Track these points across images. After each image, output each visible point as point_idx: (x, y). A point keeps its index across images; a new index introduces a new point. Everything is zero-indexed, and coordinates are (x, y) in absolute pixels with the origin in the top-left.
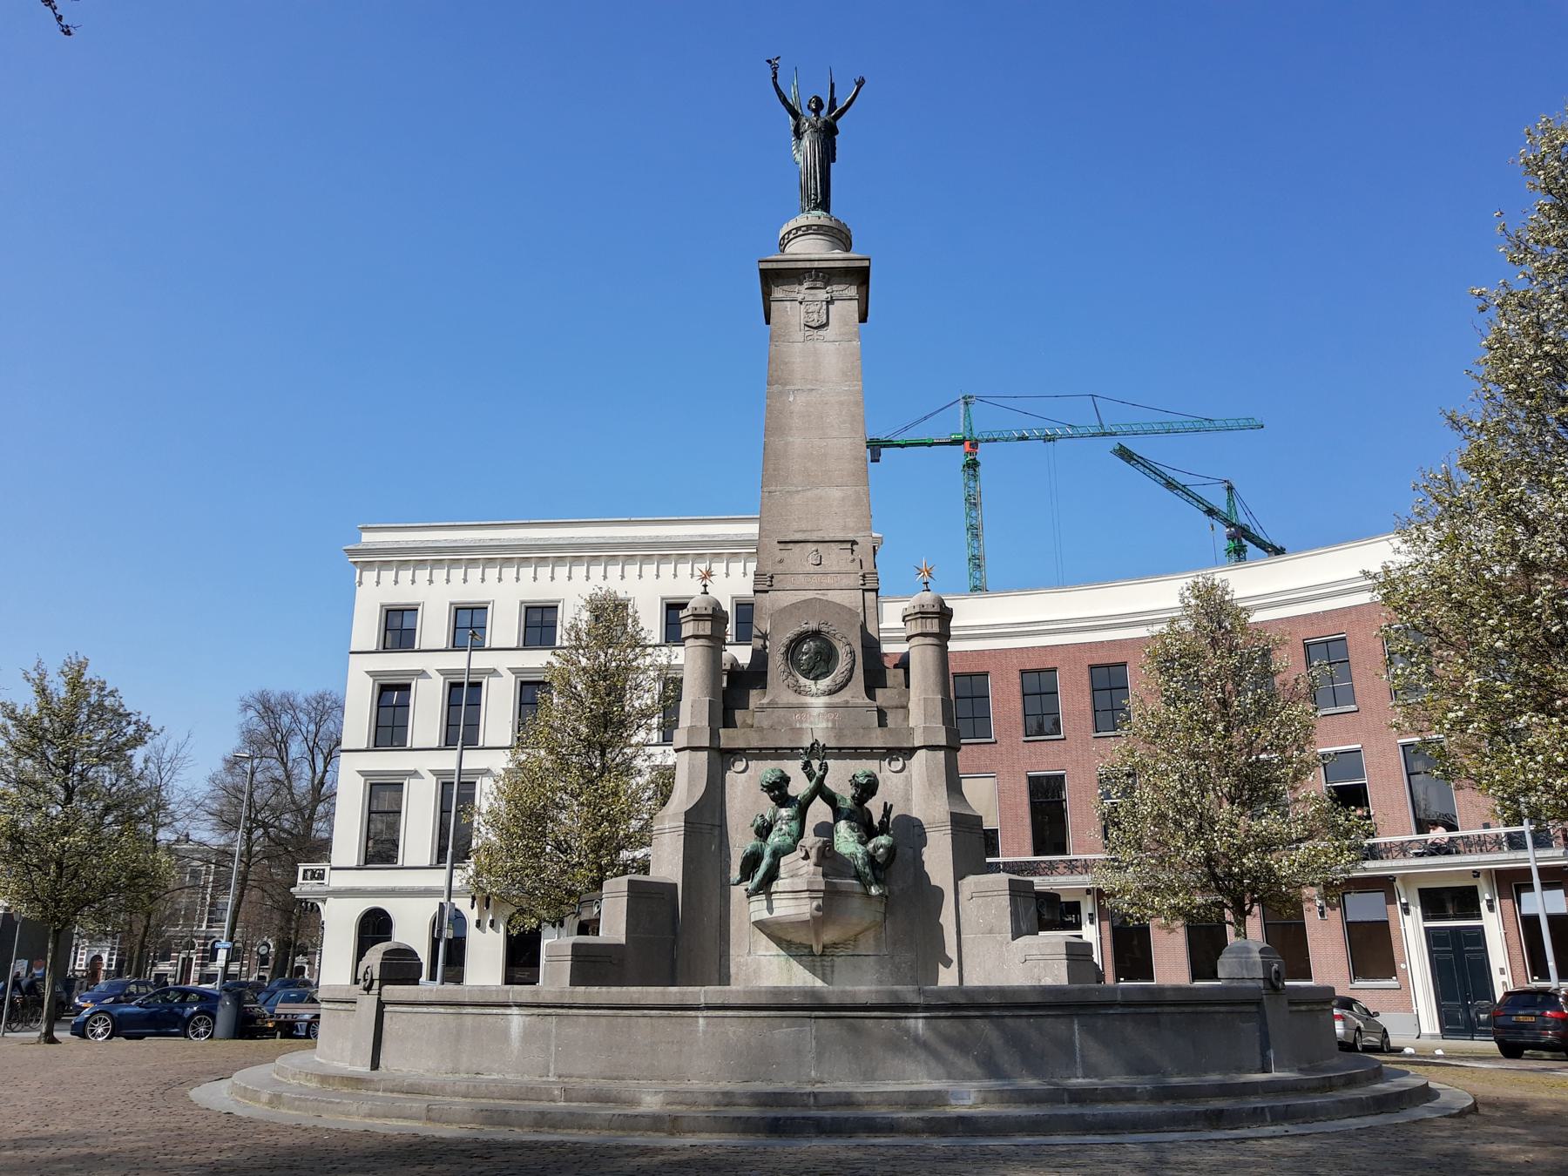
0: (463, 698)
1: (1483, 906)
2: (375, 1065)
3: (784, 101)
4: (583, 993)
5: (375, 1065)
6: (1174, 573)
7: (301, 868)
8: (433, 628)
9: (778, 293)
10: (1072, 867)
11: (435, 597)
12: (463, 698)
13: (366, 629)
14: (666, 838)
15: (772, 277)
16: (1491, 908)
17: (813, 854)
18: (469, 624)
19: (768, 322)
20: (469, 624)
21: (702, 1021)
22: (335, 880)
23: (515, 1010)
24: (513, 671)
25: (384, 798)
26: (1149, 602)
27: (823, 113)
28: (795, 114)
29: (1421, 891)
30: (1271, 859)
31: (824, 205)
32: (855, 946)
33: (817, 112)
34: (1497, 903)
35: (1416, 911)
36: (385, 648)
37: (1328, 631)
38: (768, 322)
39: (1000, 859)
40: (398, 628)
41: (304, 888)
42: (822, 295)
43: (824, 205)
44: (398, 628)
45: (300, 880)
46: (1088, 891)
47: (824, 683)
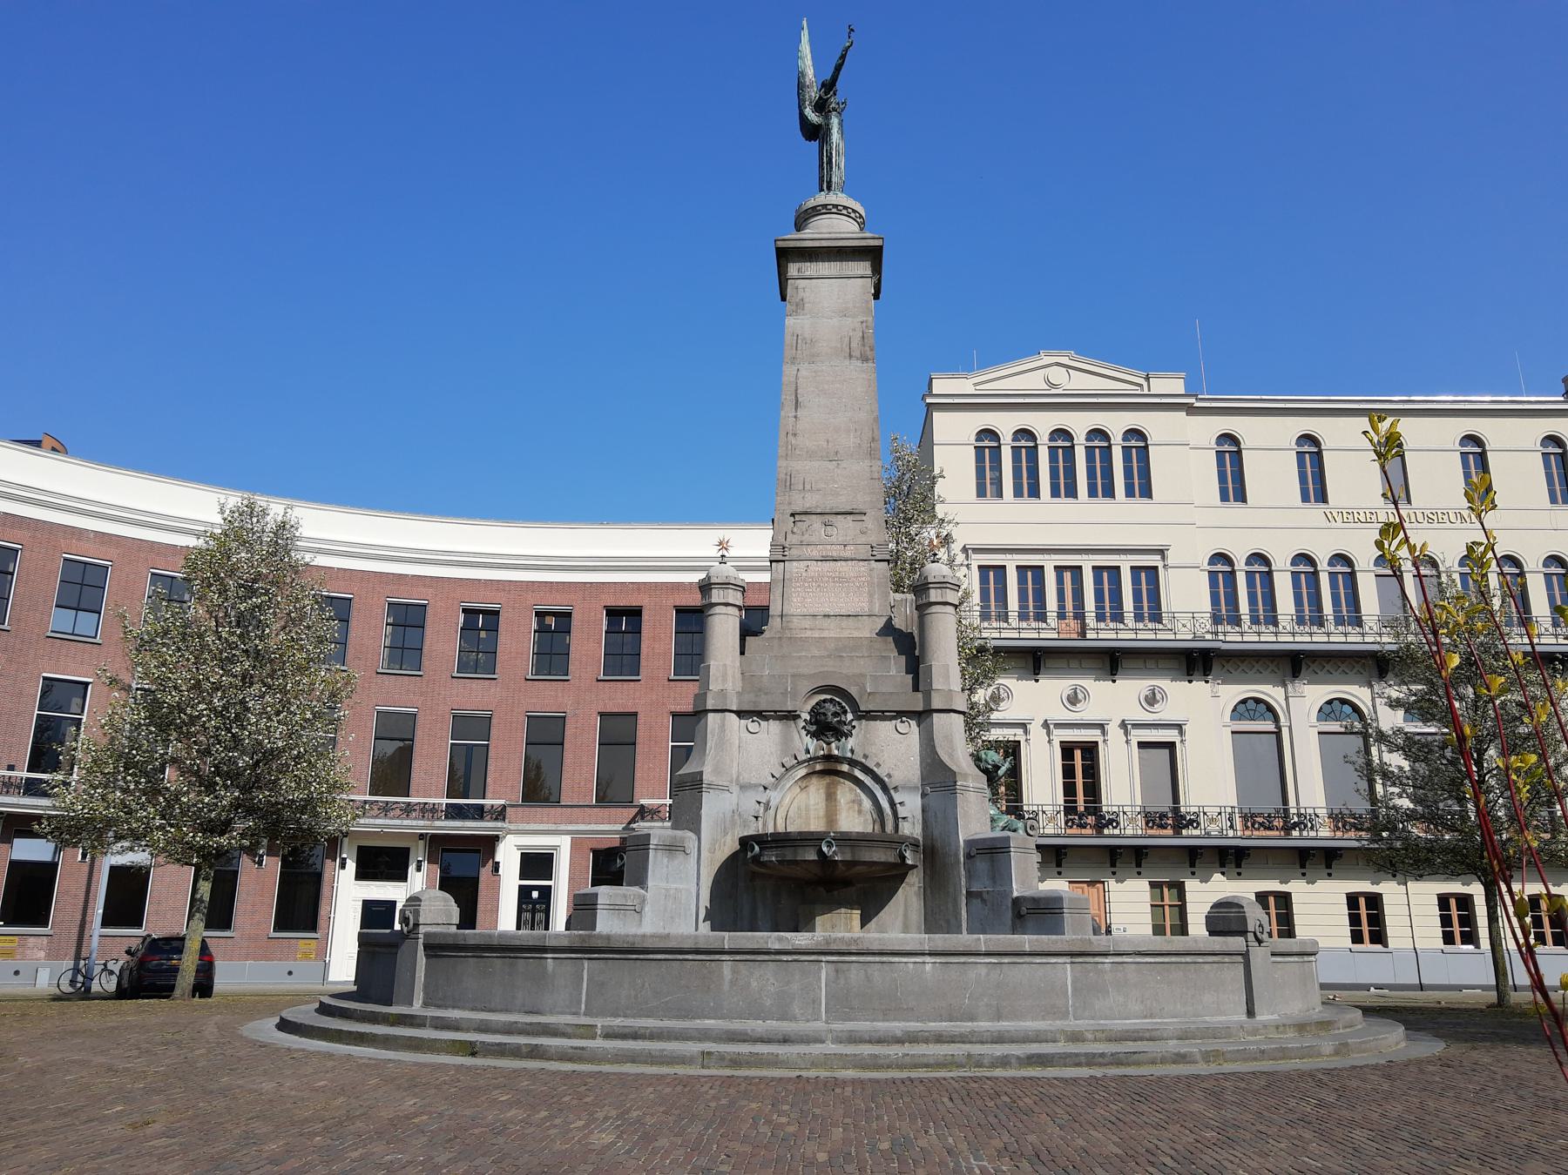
1: (412, 868)
2: (1251, 1013)
4: (729, 939)
5: (1251, 1013)
6: (360, 507)
9: (793, 269)
10: (408, 810)
14: (972, 796)
15: (785, 255)
16: (419, 869)
19: (784, 299)
21: (727, 968)
23: (928, 959)
26: (180, 510)
29: (359, 848)
30: (642, 826)
34: (425, 865)
35: (351, 866)
37: (556, 603)
38: (784, 299)
39: (487, 802)
46: (422, 836)
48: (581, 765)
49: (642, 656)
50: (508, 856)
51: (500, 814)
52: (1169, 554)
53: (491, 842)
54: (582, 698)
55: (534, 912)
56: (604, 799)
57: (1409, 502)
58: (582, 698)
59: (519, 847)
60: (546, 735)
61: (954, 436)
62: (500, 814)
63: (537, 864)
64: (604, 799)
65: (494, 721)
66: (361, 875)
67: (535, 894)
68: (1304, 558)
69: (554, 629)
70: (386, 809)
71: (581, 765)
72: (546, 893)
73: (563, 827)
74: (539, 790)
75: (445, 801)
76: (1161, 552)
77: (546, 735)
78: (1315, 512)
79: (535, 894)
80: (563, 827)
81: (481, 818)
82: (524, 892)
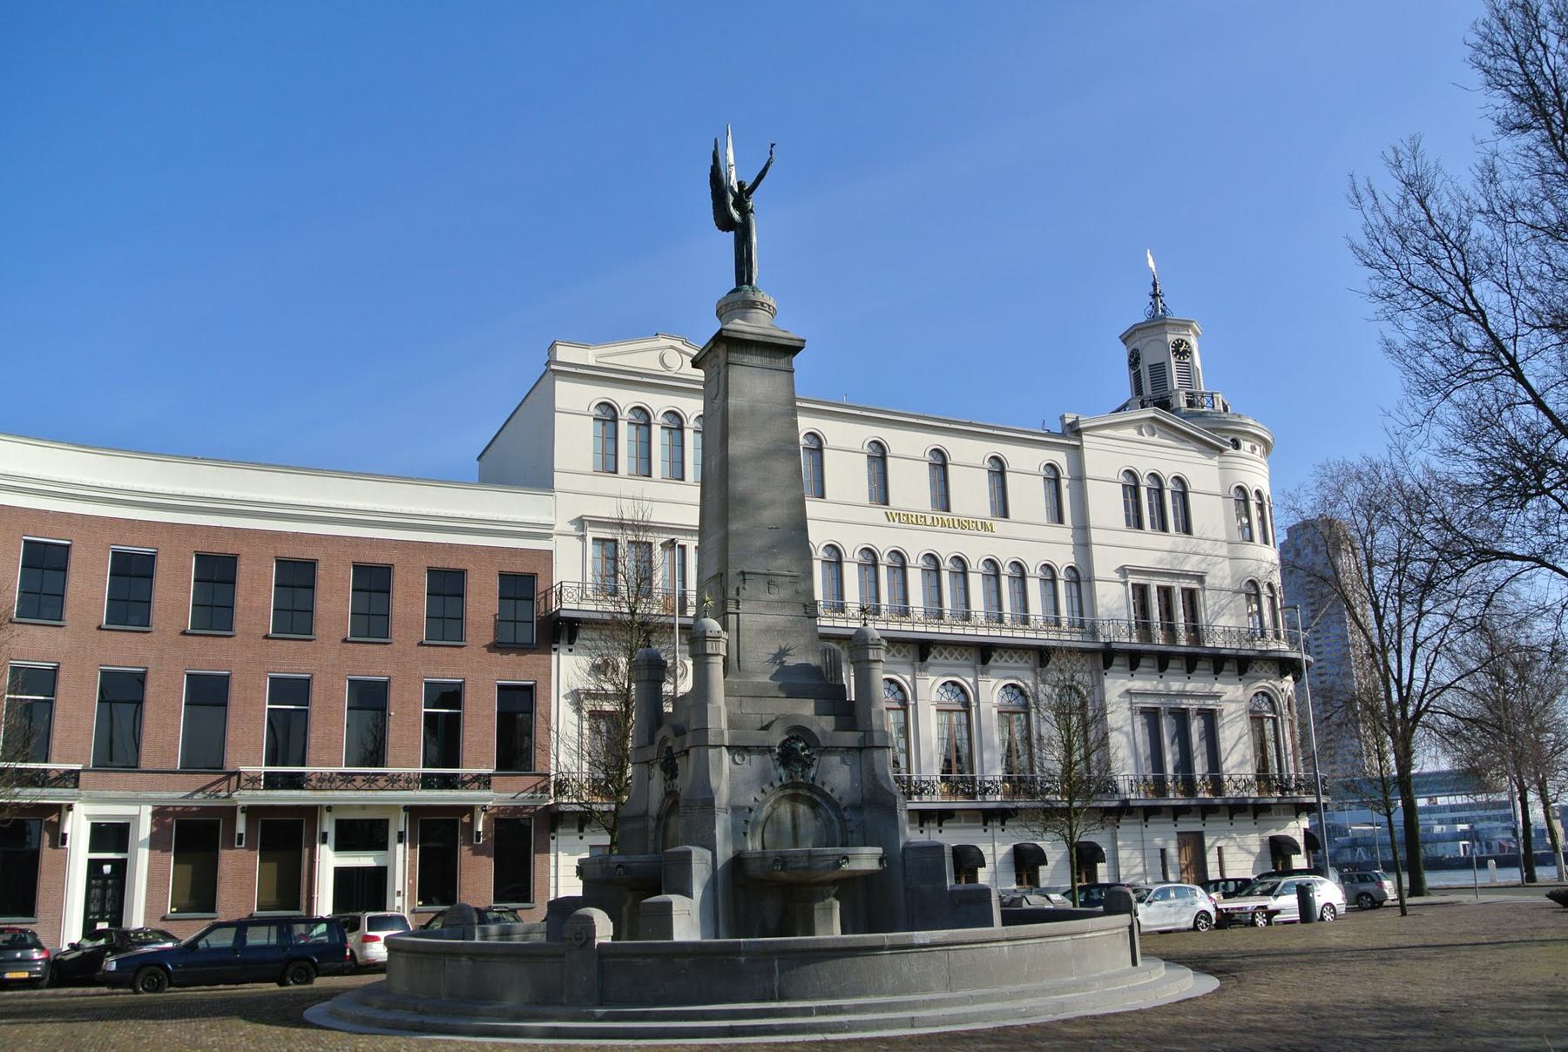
48: (165, 723)
49: (237, 611)
50: (78, 827)
51: (71, 779)
52: (1207, 579)
53: (60, 810)
54: (167, 655)
55: (104, 887)
56: (189, 767)
57: (821, 495)
58: (167, 655)
59: (89, 817)
60: (123, 693)
61: (575, 400)
62: (71, 779)
63: (110, 836)
64: (189, 767)
65: (62, 674)
66: (340, 846)
67: (107, 869)
68: (868, 551)
69: (133, 575)
70: (371, 780)
71: (165, 723)
72: (120, 868)
73: (143, 795)
74: (118, 752)
75: (264, 769)
76: (1200, 578)
77: (370, 699)
78: (878, 513)
79: (107, 869)
80: (143, 795)
81: (300, 787)
82: (94, 867)
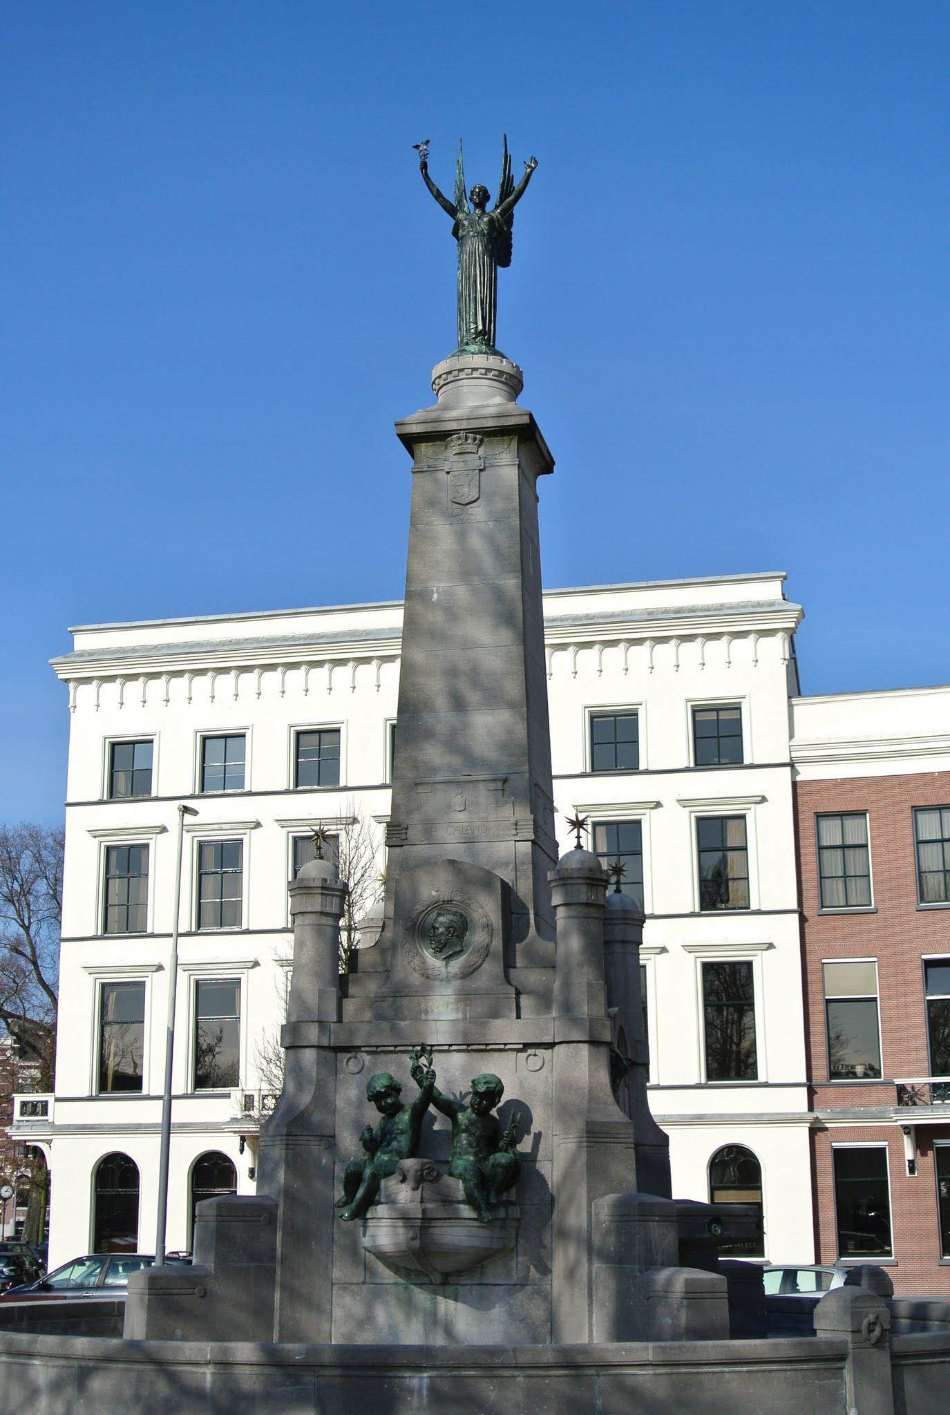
0: (220, 862)
3: (438, 196)
7: (18, 1099)
8: (174, 769)
11: (172, 722)
12: (220, 862)
13: (86, 771)
17: (410, 1176)
18: (220, 758)
20: (220, 758)
22: (59, 1113)
24: (283, 823)
25: (121, 1004)
27: (489, 206)
28: (452, 210)
31: (487, 338)
32: (482, 1274)
33: (481, 205)
36: (113, 795)
40: (128, 769)
41: (22, 1130)
42: (473, 461)
43: (487, 338)
44: (128, 769)
45: (17, 1115)
47: (456, 965)
